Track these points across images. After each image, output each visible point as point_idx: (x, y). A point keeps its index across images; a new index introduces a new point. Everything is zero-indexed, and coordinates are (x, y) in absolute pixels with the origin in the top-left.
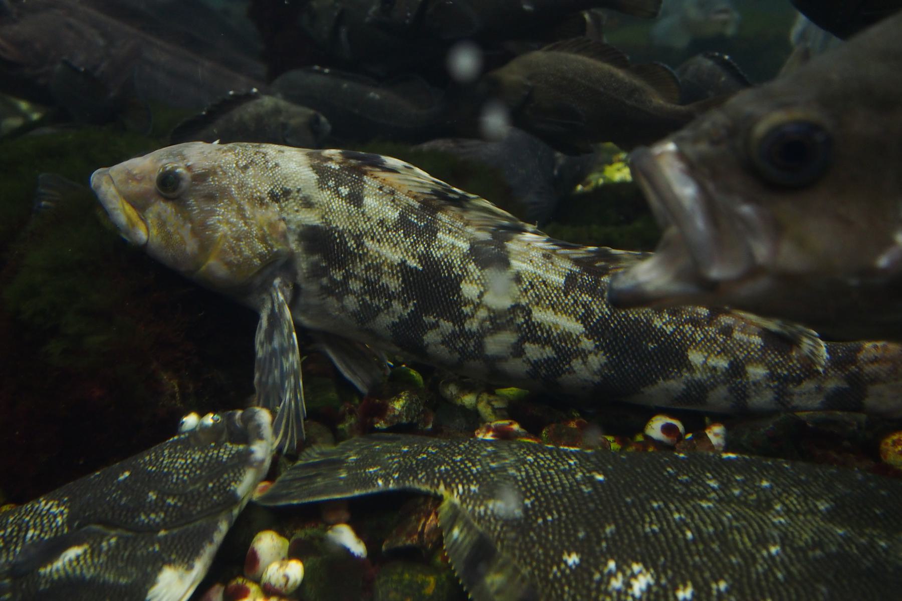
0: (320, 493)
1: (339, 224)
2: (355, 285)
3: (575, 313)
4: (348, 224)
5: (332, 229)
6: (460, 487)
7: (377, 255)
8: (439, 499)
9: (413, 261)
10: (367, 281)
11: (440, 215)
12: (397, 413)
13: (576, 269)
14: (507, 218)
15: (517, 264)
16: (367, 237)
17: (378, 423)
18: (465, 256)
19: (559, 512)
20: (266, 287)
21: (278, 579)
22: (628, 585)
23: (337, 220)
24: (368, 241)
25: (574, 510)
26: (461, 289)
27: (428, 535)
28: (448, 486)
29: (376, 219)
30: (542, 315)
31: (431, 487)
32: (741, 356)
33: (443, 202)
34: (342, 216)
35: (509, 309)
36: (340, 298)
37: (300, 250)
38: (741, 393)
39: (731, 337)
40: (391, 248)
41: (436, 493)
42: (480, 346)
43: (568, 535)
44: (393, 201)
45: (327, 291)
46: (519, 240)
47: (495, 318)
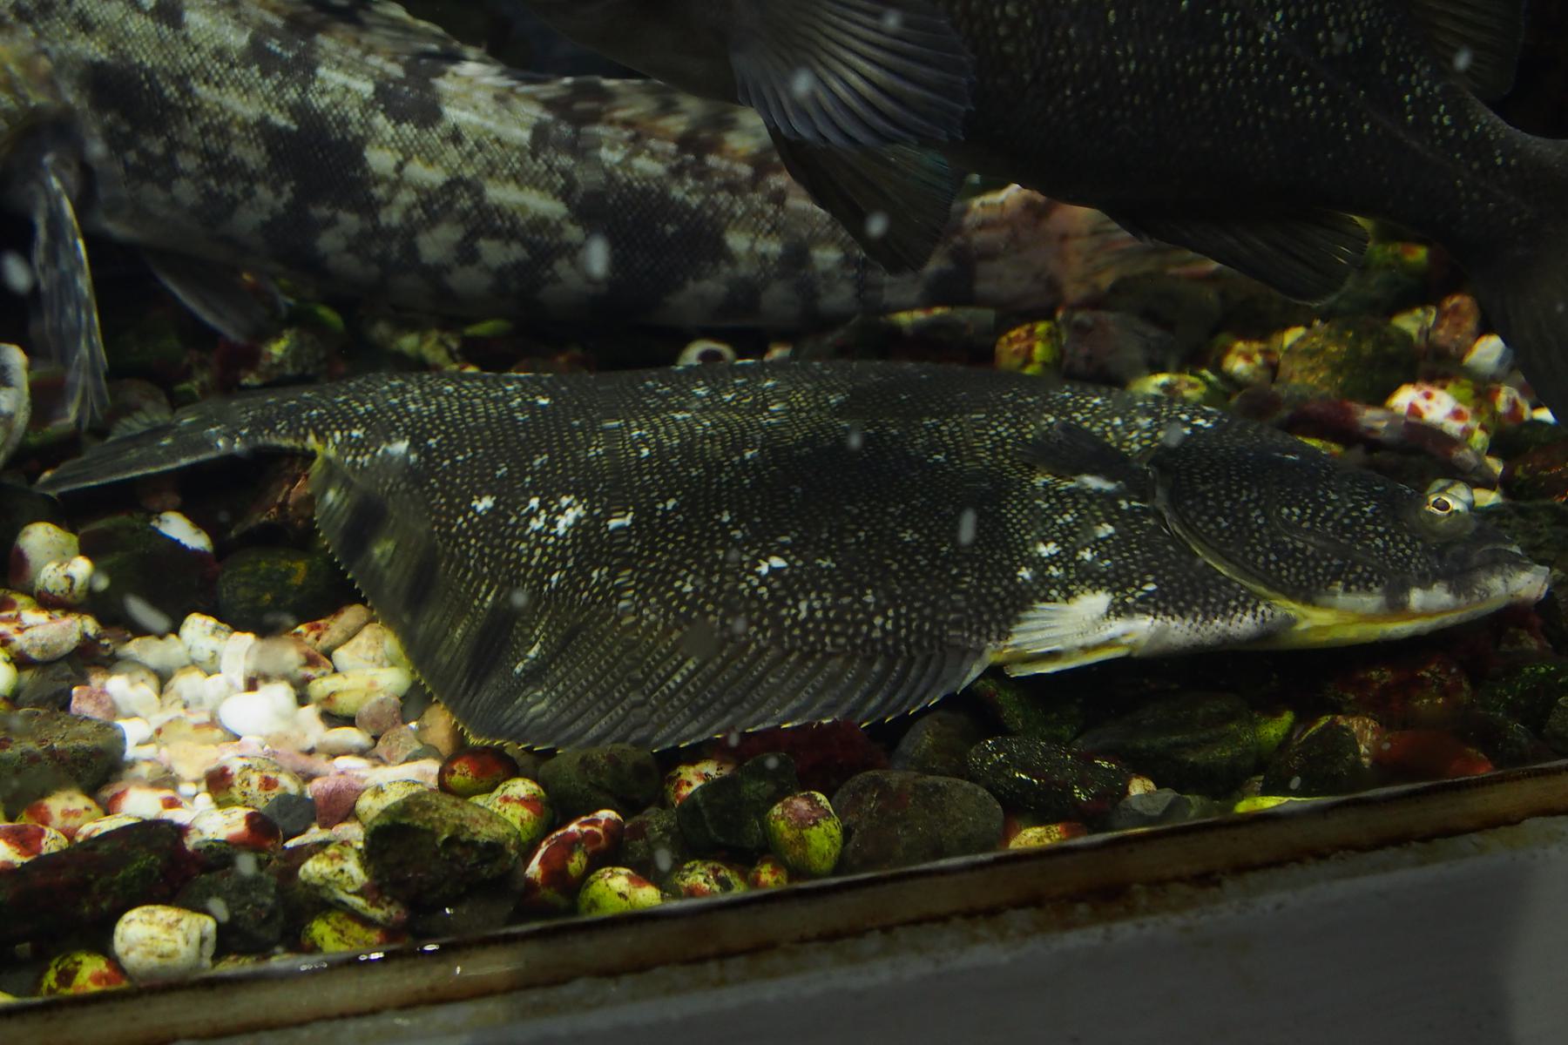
0: (129, 468)
1: (144, 58)
2: (188, 162)
3: (550, 186)
4: (161, 57)
5: (133, 67)
6: (338, 434)
7: (217, 109)
8: (312, 456)
9: (238, 101)
10: (206, 154)
11: (320, 38)
12: (275, 360)
13: (548, 117)
14: (435, 37)
15: (454, 114)
16: (196, 79)
17: (245, 377)
18: (367, 106)
19: (474, 450)
20: (33, 171)
21: (56, 583)
22: (552, 523)
23: (140, 51)
24: (199, 85)
25: (496, 443)
26: (365, 159)
27: (295, 508)
28: (320, 436)
29: (208, 47)
30: (500, 193)
31: (296, 441)
32: (805, 234)
33: (323, 16)
34: (150, 45)
35: (441, 188)
36: (166, 185)
37: (86, 105)
38: (808, 290)
39: (784, 207)
40: (240, 96)
41: (304, 449)
42: (411, 250)
43: (482, 476)
44: (237, 17)
45: (138, 174)
46: (455, 75)
47: (431, 201)
